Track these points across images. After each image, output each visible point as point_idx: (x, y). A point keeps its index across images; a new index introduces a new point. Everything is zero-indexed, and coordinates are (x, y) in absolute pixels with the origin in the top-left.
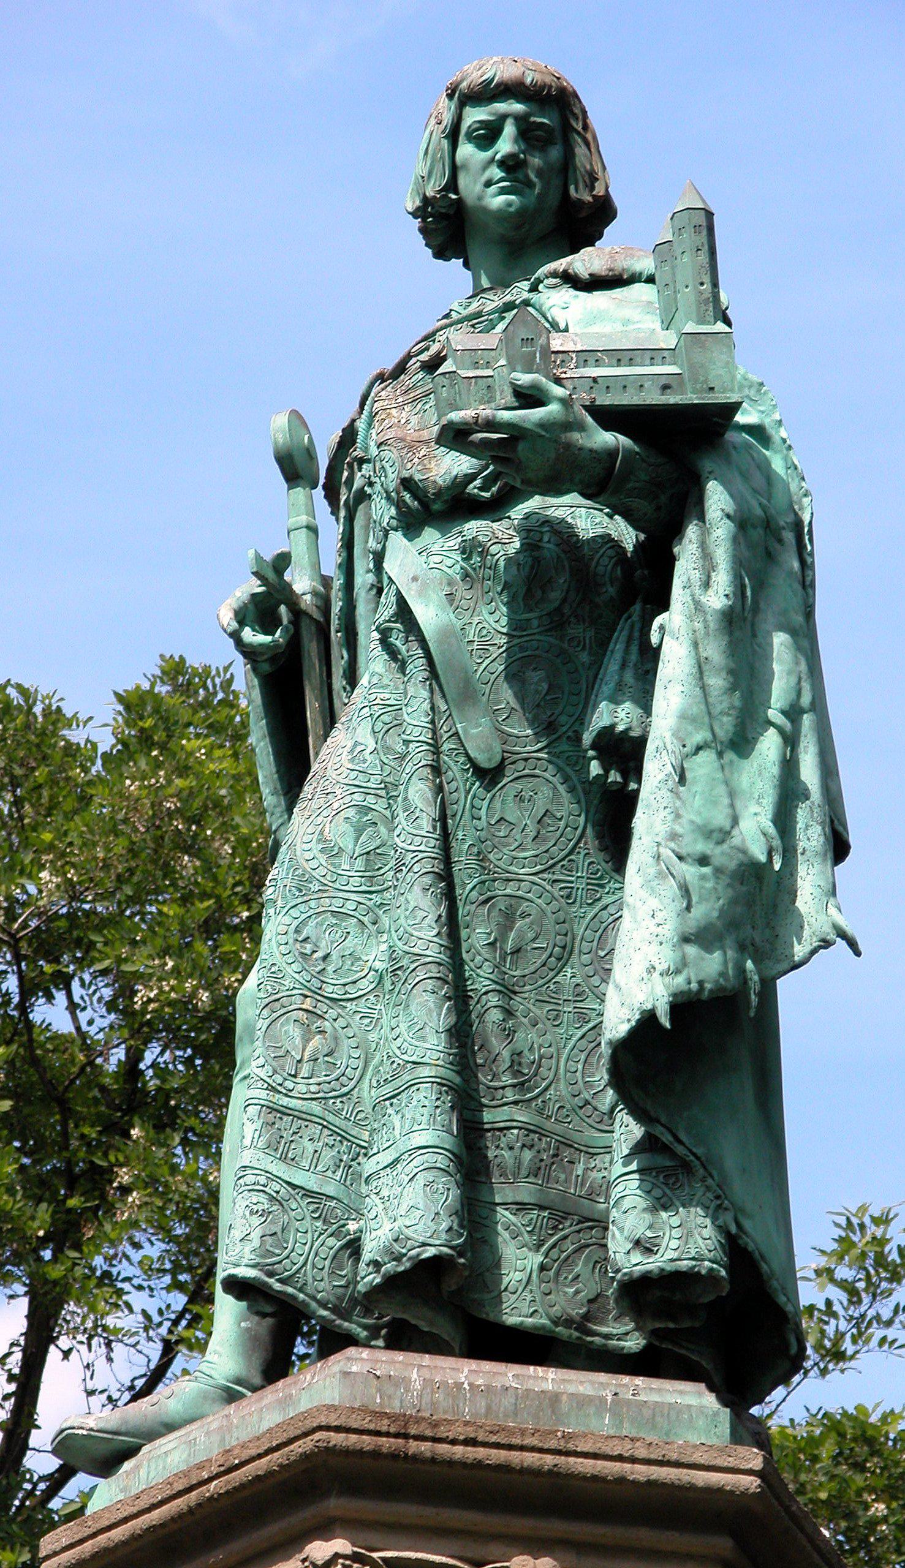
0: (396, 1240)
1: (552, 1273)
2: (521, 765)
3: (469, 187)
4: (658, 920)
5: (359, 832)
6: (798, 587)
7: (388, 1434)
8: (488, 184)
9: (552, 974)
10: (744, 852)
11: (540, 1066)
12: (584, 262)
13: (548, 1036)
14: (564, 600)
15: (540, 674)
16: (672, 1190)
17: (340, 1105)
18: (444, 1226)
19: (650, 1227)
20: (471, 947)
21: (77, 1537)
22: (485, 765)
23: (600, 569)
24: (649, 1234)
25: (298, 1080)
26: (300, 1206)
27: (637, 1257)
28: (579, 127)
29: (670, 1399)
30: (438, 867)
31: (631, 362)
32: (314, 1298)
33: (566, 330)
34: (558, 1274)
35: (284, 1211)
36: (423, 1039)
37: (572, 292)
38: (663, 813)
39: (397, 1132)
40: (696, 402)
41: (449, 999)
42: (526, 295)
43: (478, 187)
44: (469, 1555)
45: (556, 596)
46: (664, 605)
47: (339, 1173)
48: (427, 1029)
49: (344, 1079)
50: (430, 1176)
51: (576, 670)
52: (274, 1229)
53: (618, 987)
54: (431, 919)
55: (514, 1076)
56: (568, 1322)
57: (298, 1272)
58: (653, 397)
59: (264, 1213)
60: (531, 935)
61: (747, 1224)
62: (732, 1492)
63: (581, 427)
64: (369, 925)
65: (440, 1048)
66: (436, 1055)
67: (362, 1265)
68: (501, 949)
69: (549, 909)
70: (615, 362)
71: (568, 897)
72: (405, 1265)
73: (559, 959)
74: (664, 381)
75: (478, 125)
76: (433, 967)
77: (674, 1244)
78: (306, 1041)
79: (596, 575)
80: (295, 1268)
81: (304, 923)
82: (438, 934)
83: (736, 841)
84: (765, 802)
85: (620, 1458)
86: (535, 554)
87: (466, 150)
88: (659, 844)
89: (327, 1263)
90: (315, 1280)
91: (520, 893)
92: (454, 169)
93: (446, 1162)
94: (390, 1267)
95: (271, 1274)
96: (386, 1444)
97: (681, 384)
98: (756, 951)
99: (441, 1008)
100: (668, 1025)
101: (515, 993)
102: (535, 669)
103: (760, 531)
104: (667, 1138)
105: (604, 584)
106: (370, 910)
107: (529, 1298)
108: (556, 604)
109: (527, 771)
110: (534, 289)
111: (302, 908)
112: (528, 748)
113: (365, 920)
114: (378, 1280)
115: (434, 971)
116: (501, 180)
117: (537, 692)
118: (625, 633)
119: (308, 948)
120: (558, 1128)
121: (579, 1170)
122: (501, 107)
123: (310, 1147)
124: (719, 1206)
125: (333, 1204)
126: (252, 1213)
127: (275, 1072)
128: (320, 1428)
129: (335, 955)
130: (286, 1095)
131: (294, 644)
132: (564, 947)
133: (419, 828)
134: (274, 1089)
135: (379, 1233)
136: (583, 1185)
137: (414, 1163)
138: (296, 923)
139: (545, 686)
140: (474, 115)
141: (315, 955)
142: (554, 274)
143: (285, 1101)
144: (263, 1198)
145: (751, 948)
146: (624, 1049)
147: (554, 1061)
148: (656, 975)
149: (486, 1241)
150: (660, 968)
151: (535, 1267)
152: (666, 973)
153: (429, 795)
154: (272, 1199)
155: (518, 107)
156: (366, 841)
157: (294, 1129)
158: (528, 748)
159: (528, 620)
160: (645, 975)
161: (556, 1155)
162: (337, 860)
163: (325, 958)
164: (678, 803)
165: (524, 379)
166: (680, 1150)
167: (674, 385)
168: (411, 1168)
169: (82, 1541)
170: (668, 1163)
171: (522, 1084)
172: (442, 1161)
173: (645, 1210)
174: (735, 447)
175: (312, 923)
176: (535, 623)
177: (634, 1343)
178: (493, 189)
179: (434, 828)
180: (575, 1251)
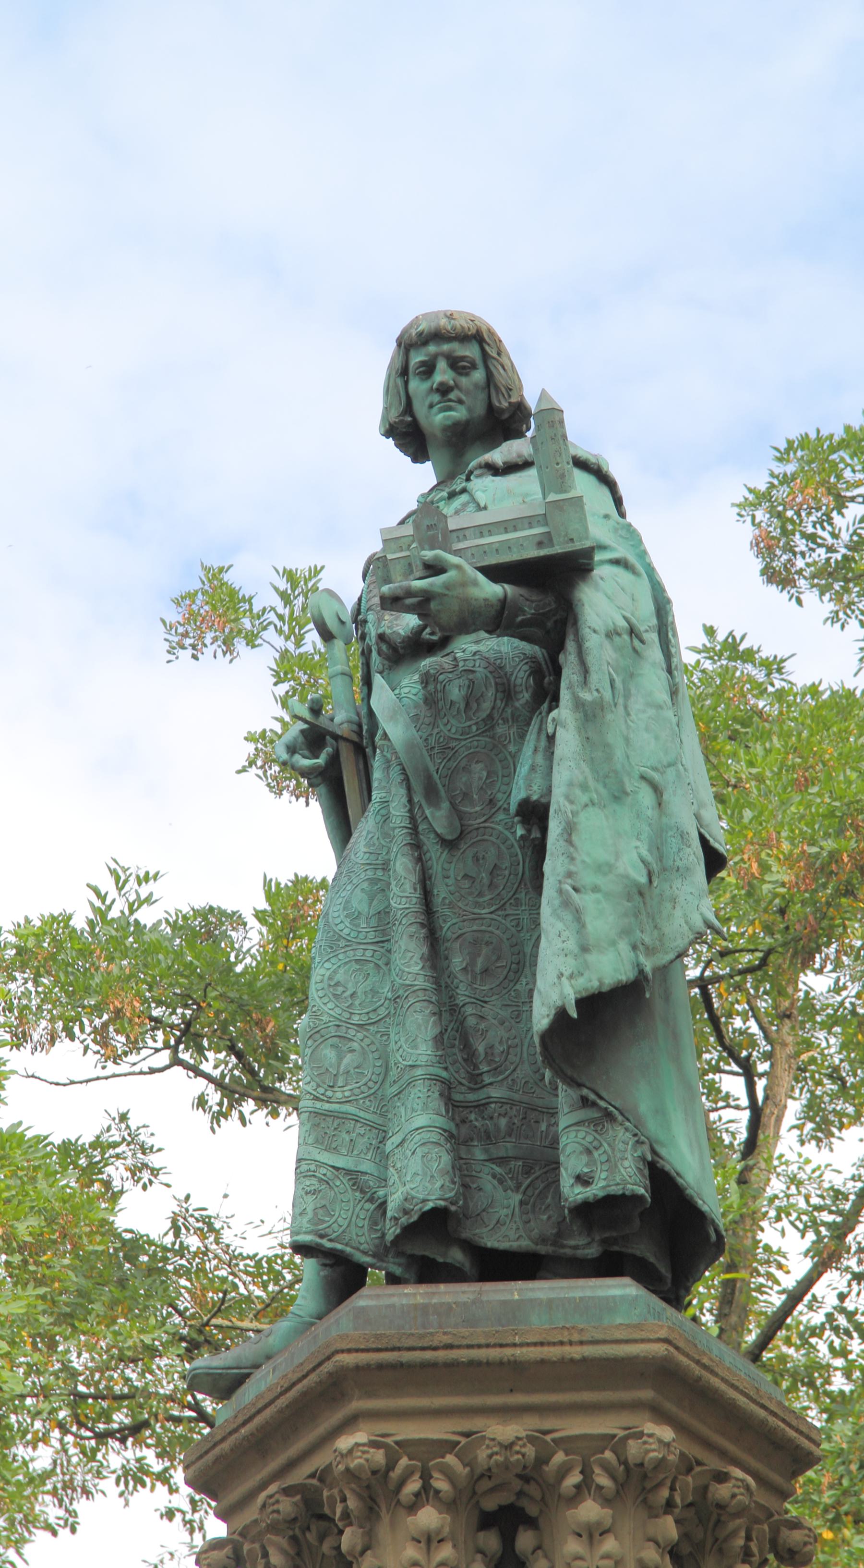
0: (406, 1200)
1: (529, 1207)
2: (475, 833)
4: (563, 938)
5: (371, 900)
6: (664, 675)
8: (431, 406)
9: (512, 984)
10: (627, 877)
11: (508, 1053)
12: (498, 455)
13: (513, 1031)
14: (493, 708)
15: (480, 766)
17: (368, 1103)
18: (438, 1184)
19: (587, 1165)
20: (451, 973)
21: (203, 1450)
22: (449, 837)
23: (519, 681)
24: (586, 1170)
25: (336, 1089)
26: (342, 1183)
27: (578, 1189)
28: (495, 355)
30: (421, 918)
31: (515, 529)
32: (358, 1249)
33: (485, 508)
34: (534, 1205)
35: (331, 1188)
36: (415, 1047)
37: (491, 478)
38: (562, 858)
39: (403, 1119)
41: (434, 1014)
42: (464, 484)
44: (460, 1430)
45: (487, 705)
47: (370, 1154)
48: (419, 1040)
49: (371, 1084)
50: (425, 1149)
51: (506, 758)
52: (323, 1202)
53: (540, 992)
54: (417, 956)
55: (489, 1064)
56: (543, 1240)
57: (344, 1232)
58: (532, 553)
59: (314, 1192)
60: (494, 958)
61: (663, 1152)
62: (645, 1358)
63: (475, 583)
64: (384, 967)
65: (429, 1052)
66: (425, 1058)
67: (388, 1221)
68: (472, 971)
69: (505, 937)
70: (502, 530)
71: (518, 925)
72: (415, 1218)
73: (516, 972)
74: (537, 539)
76: (420, 993)
77: (604, 1175)
78: (340, 1058)
79: (515, 686)
80: (341, 1230)
81: (335, 972)
82: (423, 967)
83: (621, 870)
84: (642, 837)
86: (471, 676)
87: (416, 386)
88: (560, 882)
89: (366, 1222)
90: (357, 1235)
91: (483, 928)
93: (439, 1136)
94: (404, 1220)
95: (322, 1236)
97: (551, 540)
98: (647, 948)
99: (428, 1021)
100: (574, 1014)
101: (485, 1002)
102: (477, 762)
103: (626, 637)
104: (592, 1097)
105: (521, 692)
106: (383, 955)
107: (514, 1227)
108: (488, 712)
109: (479, 838)
110: (468, 479)
111: (333, 960)
112: (479, 821)
113: (380, 963)
114: (398, 1231)
115: (421, 995)
116: (439, 402)
117: (480, 779)
118: (537, 727)
119: (340, 989)
120: (525, 1098)
121: (543, 1127)
122: (432, 348)
123: (347, 1138)
124: (637, 1142)
125: (366, 1178)
126: (307, 1193)
127: (318, 1086)
128: (337, 1352)
129: (359, 993)
130: (328, 1102)
131: (335, 760)
132: (518, 963)
133: (403, 891)
134: (316, 1099)
135: (395, 1196)
136: (546, 1137)
137: (415, 1141)
138: (328, 973)
139: (485, 774)
140: (417, 358)
141: (346, 994)
142: (480, 466)
143: (327, 1106)
144: (314, 1181)
145: (641, 947)
146: (547, 1036)
147: (519, 1049)
148: (564, 979)
149: (481, 1189)
150: (567, 974)
151: (517, 1204)
152: (571, 977)
153: (410, 866)
154: (321, 1180)
156: (377, 905)
157: (335, 1125)
158: (479, 821)
159: (470, 726)
160: (556, 980)
161: (525, 1118)
162: (357, 922)
163: (353, 995)
164: (572, 849)
165: (428, 554)
166: (602, 1104)
167: (546, 541)
168: (412, 1146)
169: (207, 1452)
170: (596, 1115)
171: (496, 1069)
172: (434, 1137)
173: (581, 1153)
174: (602, 579)
175: (341, 971)
176: (474, 728)
177: (593, 1251)
178: (435, 409)
179: (415, 889)
180: (544, 1188)
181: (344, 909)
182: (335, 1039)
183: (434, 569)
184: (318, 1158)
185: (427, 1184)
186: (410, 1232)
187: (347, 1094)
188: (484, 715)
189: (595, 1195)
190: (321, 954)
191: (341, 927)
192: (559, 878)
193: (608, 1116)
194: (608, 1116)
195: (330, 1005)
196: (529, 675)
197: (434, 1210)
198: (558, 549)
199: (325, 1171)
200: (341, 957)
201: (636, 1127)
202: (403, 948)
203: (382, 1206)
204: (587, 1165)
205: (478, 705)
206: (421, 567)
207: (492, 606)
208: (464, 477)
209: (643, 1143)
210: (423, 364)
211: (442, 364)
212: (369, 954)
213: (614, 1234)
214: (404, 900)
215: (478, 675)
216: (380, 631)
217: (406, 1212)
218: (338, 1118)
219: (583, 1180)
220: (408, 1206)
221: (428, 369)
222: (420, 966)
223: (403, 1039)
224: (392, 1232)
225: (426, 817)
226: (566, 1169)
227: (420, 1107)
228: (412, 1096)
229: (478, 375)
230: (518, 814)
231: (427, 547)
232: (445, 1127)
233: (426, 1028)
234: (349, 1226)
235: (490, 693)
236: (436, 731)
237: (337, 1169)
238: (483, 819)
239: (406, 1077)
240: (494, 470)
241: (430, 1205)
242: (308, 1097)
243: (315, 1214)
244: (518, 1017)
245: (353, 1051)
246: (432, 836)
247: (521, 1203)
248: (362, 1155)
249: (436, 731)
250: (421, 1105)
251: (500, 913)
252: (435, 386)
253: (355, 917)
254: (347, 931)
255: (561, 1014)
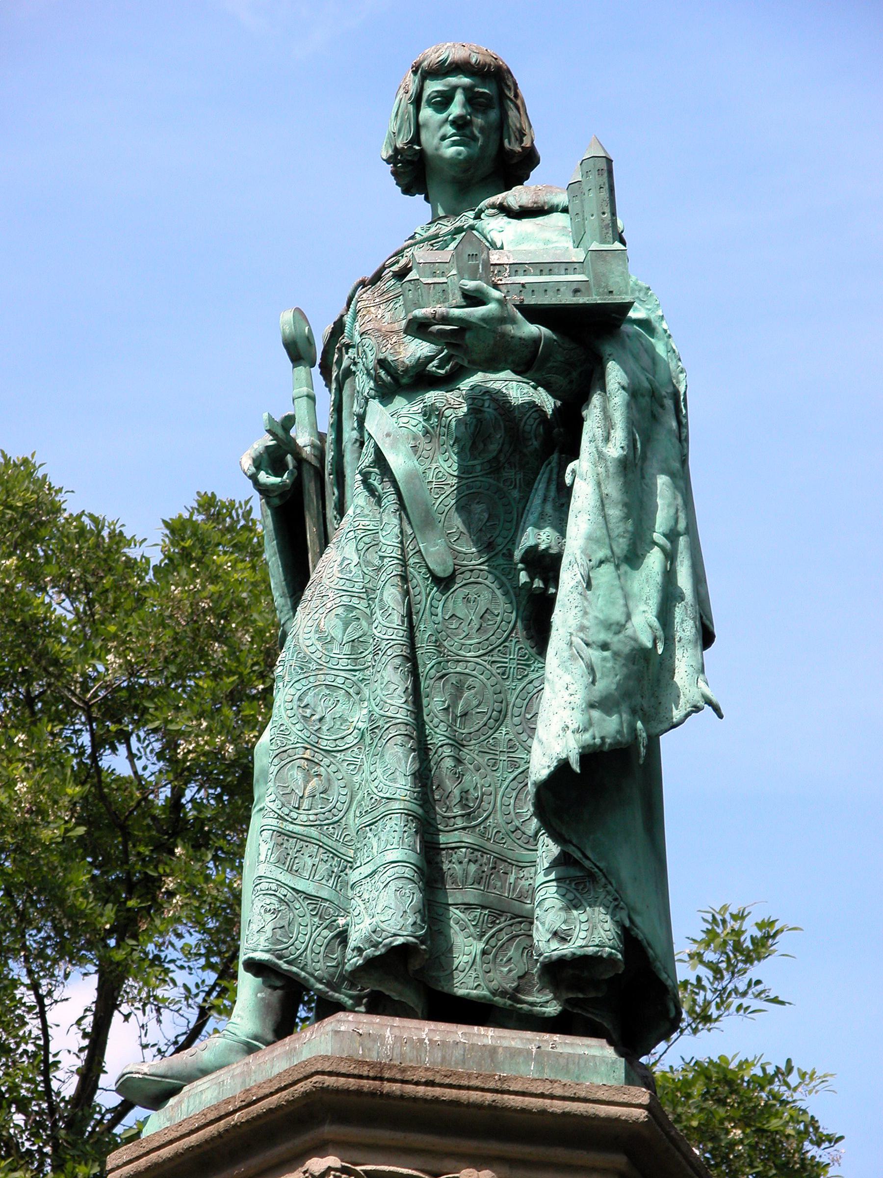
0: (374, 932)
1: (491, 956)
3: (429, 140)
4: (570, 691)
5: (346, 625)
7: (368, 1078)
8: (443, 138)
9: (491, 732)
10: (635, 639)
12: (516, 197)
14: (500, 451)
16: (581, 894)
17: (332, 831)
18: (410, 921)
19: (565, 922)
21: (135, 1155)
22: (441, 574)
23: (528, 428)
24: (564, 927)
25: (301, 811)
26: (302, 906)
27: (554, 944)
28: (512, 96)
29: (580, 1051)
31: (550, 272)
32: (312, 975)
34: (495, 957)
35: (290, 910)
37: (506, 219)
39: (375, 850)
40: (599, 302)
42: (471, 222)
43: (436, 141)
46: (575, 454)
47: (331, 881)
48: (398, 773)
51: (509, 504)
52: (283, 923)
54: (401, 690)
56: (503, 993)
57: (300, 955)
58: (567, 299)
61: (638, 920)
63: (513, 321)
64: (354, 695)
72: (381, 951)
73: (496, 721)
74: (575, 286)
75: (435, 94)
76: (402, 727)
77: (583, 934)
79: (524, 431)
80: (298, 952)
81: (305, 693)
83: (629, 632)
84: (651, 602)
85: (542, 1096)
86: (479, 416)
87: (427, 113)
88: (571, 634)
89: (322, 949)
91: (467, 671)
92: (418, 127)
93: (412, 873)
94: (369, 952)
95: (280, 957)
96: (366, 1084)
97: (588, 288)
98: (645, 714)
99: (408, 757)
100: (578, 770)
101: (463, 746)
102: (478, 503)
104: (577, 855)
105: (530, 439)
108: (495, 454)
109: (472, 580)
110: (478, 217)
111: (304, 682)
112: (473, 562)
113: (351, 691)
114: (361, 962)
115: (403, 729)
117: (480, 520)
118: (546, 476)
119: (308, 712)
120: (496, 848)
121: (512, 879)
122: (453, 80)
123: (309, 862)
125: (327, 904)
127: (283, 805)
130: (292, 823)
132: (500, 712)
134: (282, 818)
136: (514, 890)
138: (299, 693)
139: (486, 515)
140: (433, 87)
142: (493, 206)
143: (291, 827)
144: (274, 900)
145: (640, 713)
146: (544, 788)
147: (492, 797)
148: (569, 732)
150: (572, 727)
151: (479, 952)
152: (577, 731)
154: (281, 901)
155: (466, 81)
156: (352, 632)
157: (297, 848)
158: (473, 562)
160: (561, 732)
161: (494, 868)
162: (329, 646)
163: (321, 719)
164: (586, 603)
166: (587, 864)
167: (583, 289)
168: (385, 878)
169: (138, 1158)
171: (469, 814)
172: (408, 872)
174: (628, 336)
175: (311, 694)
176: (479, 468)
177: (553, 1009)
179: (403, 622)
180: (509, 940)
181: (316, 632)
182: (303, 761)
183: (473, 299)
184: (280, 878)
185: (401, 920)
186: (371, 964)
187: (312, 818)
188: (491, 456)
189: (574, 954)
190: (290, 674)
191: (312, 649)
192: (571, 631)
193: (591, 877)
194: (591, 877)
195: (298, 726)
196: (539, 424)
197: (404, 946)
198: (595, 298)
199: (285, 892)
200: (311, 679)
201: (616, 891)
202: (386, 679)
203: (342, 937)
204: (565, 922)
205: (485, 445)
206: (458, 294)
207: (527, 346)
208: (471, 214)
209: (622, 908)
210: (440, 93)
211: (459, 97)
212: (340, 680)
213: (581, 996)
214: (390, 631)
215: (486, 415)
216: (381, 356)
217: (376, 945)
218: (301, 840)
219: (560, 936)
220: (375, 937)
221: (443, 101)
222: (403, 700)
223: (379, 772)
224: (354, 961)
225: (420, 551)
226: (543, 924)
227: (396, 841)
228: (388, 828)
229: (493, 115)
230: (522, 561)
231: (466, 276)
232: (419, 865)
233: (406, 762)
234: (306, 949)
235: (499, 436)
236: (434, 466)
237: (298, 891)
238: (479, 562)
239: (382, 809)
240: (505, 210)
241: (399, 941)
242: (272, 815)
243: (274, 934)
244: (494, 765)
245: (319, 775)
246: (424, 570)
247: (484, 952)
248: (324, 882)
249: (434, 466)
250: (397, 839)
251: (486, 658)
252: (451, 118)
253: (327, 641)
254: (319, 654)
255: (563, 766)
